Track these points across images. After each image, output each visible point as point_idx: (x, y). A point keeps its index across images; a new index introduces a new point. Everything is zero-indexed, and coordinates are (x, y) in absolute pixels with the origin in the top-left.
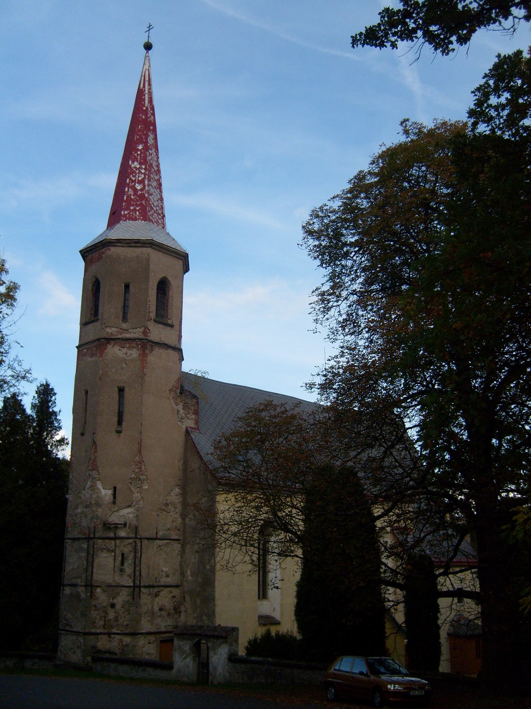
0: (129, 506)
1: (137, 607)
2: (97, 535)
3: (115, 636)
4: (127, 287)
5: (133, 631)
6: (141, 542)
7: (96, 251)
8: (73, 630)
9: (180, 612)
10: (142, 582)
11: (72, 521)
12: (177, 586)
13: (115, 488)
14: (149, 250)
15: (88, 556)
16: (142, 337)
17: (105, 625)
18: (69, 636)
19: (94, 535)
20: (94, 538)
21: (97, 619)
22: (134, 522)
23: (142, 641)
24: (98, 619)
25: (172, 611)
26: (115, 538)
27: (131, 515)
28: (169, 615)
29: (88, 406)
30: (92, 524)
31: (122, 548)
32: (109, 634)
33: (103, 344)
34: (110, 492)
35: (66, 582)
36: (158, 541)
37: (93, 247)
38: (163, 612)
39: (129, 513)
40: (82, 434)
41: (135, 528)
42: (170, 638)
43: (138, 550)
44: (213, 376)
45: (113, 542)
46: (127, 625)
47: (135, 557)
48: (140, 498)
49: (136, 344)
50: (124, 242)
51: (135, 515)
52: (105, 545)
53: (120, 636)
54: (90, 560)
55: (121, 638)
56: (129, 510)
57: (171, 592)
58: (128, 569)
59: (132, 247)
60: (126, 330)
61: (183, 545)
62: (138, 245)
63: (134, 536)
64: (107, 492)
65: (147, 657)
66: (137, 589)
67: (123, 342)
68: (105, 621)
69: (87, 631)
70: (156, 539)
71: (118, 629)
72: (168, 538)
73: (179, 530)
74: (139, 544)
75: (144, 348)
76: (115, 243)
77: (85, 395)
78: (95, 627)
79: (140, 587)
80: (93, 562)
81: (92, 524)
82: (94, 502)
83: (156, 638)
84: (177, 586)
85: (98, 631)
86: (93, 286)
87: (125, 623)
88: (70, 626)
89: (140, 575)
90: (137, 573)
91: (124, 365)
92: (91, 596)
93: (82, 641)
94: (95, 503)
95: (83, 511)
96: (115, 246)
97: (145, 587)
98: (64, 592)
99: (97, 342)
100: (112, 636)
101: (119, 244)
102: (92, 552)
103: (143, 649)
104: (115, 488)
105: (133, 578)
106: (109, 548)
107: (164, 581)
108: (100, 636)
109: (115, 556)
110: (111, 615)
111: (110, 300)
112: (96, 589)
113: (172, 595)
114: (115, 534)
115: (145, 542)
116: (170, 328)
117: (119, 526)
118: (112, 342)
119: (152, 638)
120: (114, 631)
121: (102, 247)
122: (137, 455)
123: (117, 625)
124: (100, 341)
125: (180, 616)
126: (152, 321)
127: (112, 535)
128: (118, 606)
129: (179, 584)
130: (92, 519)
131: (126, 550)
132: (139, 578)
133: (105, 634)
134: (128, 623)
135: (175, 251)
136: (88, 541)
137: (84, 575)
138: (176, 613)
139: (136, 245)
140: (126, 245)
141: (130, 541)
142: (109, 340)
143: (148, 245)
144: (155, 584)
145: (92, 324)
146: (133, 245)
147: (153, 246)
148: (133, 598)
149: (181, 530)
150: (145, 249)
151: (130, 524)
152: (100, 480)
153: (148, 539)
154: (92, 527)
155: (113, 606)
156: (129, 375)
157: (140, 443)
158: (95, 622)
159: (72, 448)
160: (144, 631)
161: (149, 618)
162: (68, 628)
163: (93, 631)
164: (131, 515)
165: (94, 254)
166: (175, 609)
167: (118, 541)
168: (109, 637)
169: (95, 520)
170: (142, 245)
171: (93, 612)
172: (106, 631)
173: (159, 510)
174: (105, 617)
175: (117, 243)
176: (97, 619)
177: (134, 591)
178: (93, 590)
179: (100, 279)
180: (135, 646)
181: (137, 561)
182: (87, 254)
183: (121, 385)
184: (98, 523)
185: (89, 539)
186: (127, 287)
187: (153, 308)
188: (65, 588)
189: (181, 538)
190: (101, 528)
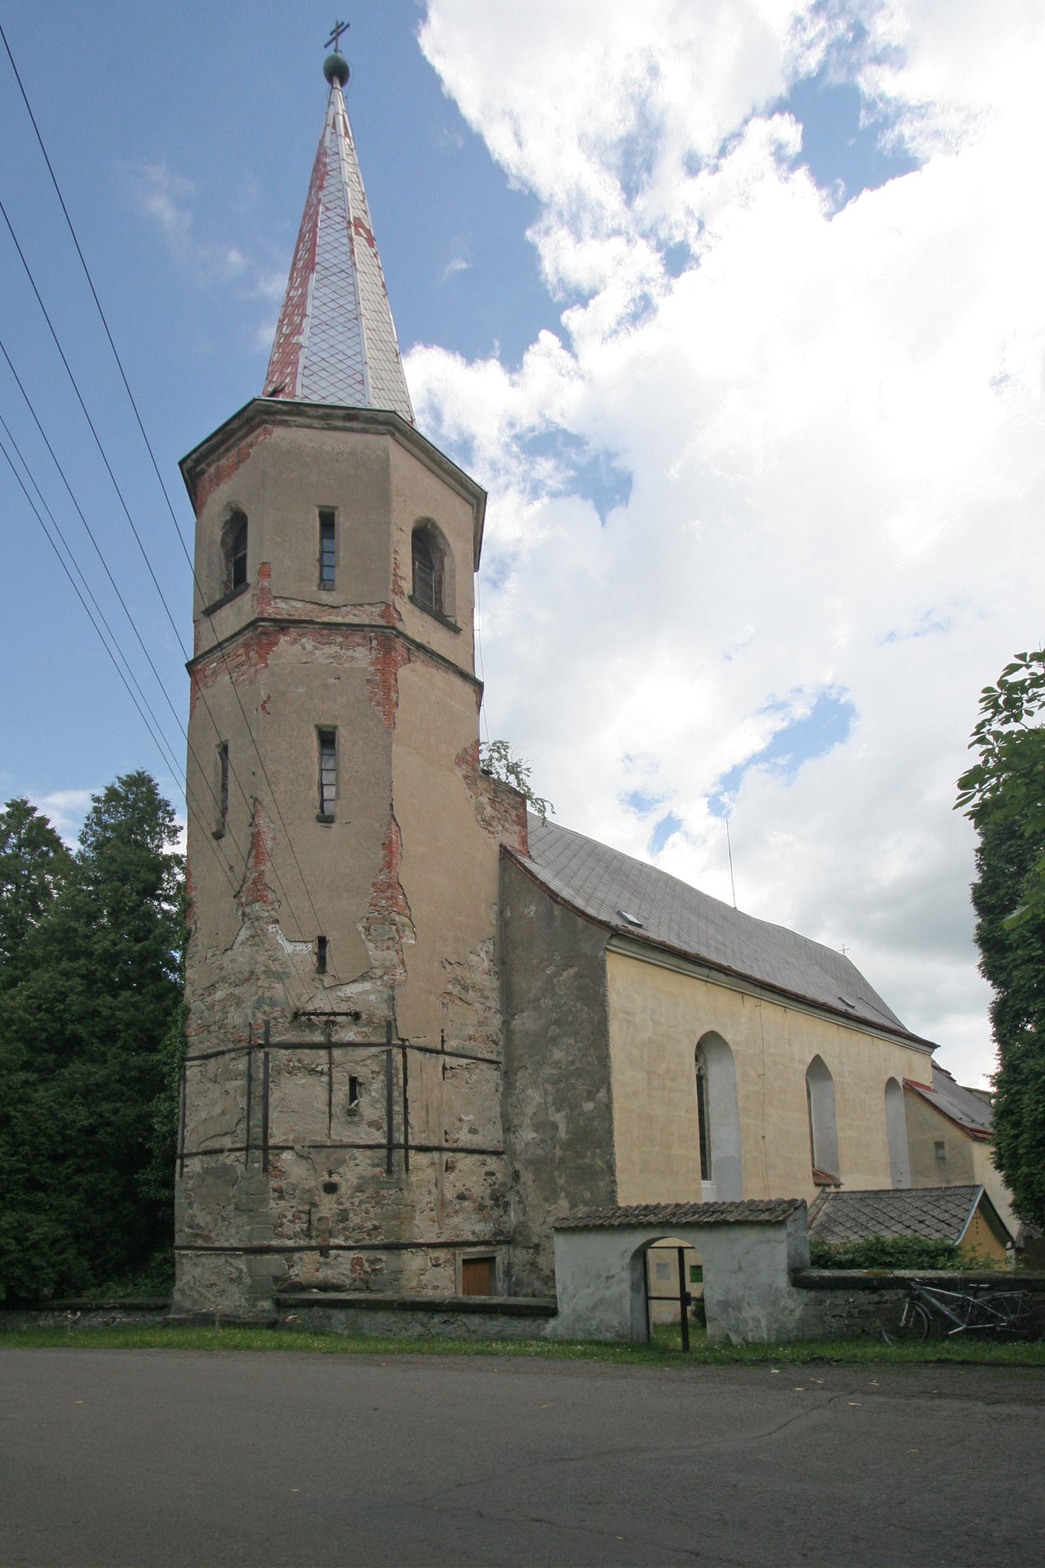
0: (364, 977)
1: (401, 1189)
2: (275, 1039)
3: (341, 1252)
4: (328, 522)
5: (392, 1240)
6: (405, 1055)
7: (228, 450)
8: (217, 1244)
9: (507, 1204)
10: (410, 1137)
11: (199, 1022)
12: (496, 1153)
13: (322, 942)
14: (387, 441)
15: (249, 1086)
16: (381, 622)
17: (309, 1229)
18: (204, 1260)
19: (267, 1039)
20: (268, 1044)
21: (285, 1217)
22: (383, 1011)
23: (414, 1262)
24: (290, 1217)
25: (489, 1202)
26: (329, 1046)
27: (373, 997)
28: (481, 1208)
29: (229, 817)
30: (259, 1015)
31: (349, 1066)
32: (324, 1250)
33: (265, 633)
34: (307, 950)
35: (190, 1147)
36: (447, 1058)
37: (219, 437)
38: (466, 1204)
39: (366, 992)
40: (218, 836)
41: (384, 1024)
42: (485, 1256)
43: (397, 1069)
44: (898, 181)
45: (323, 1053)
46: (375, 1228)
47: (389, 1085)
48: (396, 961)
49: (364, 638)
50: (312, 412)
51: (385, 996)
52: (299, 1061)
53: (355, 1252)
54: (258, 1091)
55: (359, 1255)
56: (367, 986)
57: (484, 1164)
58: (371, 1107)
59: (335, 429)
60: (332, 607)
61: (506, 1073)
62: (355, 425)
63: (384, 1040)
64: (298, 948)
65: (431, 1293)
66: (398, 1155)
67: (325, 632)
68: (309, 1222)
69: (256, 1243)
70: (442, 1052)
71: (347, 1238)
72: (468, 1054)
73: (496, 1043)
74: (398, 1058)
75: (387, 648)
76: (284, 413)
77: (222, 758)
78: (281, 1236)
79: (407, 1147)
80: (265, 1098)
81: (259, 1015)
82: (263, 969)
83: (454, 1255)
84: (496, 1153)
85: (290, 1243)
86: (225, 534)
87: (369, 1225)
88: (207, 1238)
89: (406, 1121)
90: (398, 1119)
91: (332, 681)
92: (265, 1170)
93: (243, 1267)
94: (264, 972)
95: (231, 994)
96: (284, 423)
97: (422, 1149)
98: (185, 1170)
99: (248, 634)
100: (333, 1252)
101: (299, 420)
102: (261, 1076)
103: (422, 1277)
104: (322, 942)
105: (386, 1129)
106: (314, 1066)
107: (464, 1138)
108: (296, 1256)
109: (330, 1084)
110: (328, 1206)
111: (279, 540)
112: (278, 1155)
113: (486, 1169)
114: (329, 1036)
115: (413, 1055)
116: (452, 633)
117: (340, 1019)
118: (293, 632)
119: (442, 1254)
120: (334, 1241)
121: (244, 430)
122: (382, 870)
123: (345, 1229)
124: (256, 629)
125: (506, 1212)
126: (406, 600)
127: (318, 1038)
128: (344, 1189)
129: (501, 1149)
130: (258, 1006)
131: (362, 1072)
132: (403, 1129)
133: (311, 1248)
134: (377, 1223)
135: (456, 473)
136: (249, 1054)
137: (243, 1125)
138: (498, 1206)
139: (348, 424)
140: (316, 423)
141: (374, 1050)
142: (283, 625)
143: (382, 428)
144: (445, 1145)
145: (228, 606)
146: (339, 423)
147: (397, 434)
148: (389, 1171)
149: (501, 1043)
150: (376, 437)
151: (371, 1016)
152: (277, 922)
153: (420, 1049)
154: (260, 1021)
155: (331, 1188)
156: (348, 701)
157: (388, 846)
158: (281, 1225)
159: (189, 837)
160: (421, 1241)
161: (434, 1214)
162: (200, 1243)
163: (273, 1243)
164: (373, 997)
165: (223, 461)
166: (496, 1198)
167: (337, 1053)
168: (322, 1255)
169: (267, 1008)
170: (364, 425)
171: (272, 1204)
172: (314, 1243)
173: (446, 995)
174: (309, 1213)
175: (289, 413)
176: (285, 1217)
177: (389, 1157)
178: (271, 1157)
179: (245, 509)
180: (401, 1272)
181: (396, 1094)
182: (203, 466)
183: (326, 721)
184: (276, 1014)
185: (251, 1049)
186: (328, 522)
187: (406, 569)
188: (187, 1162)
189: (501, 1059)
190: (287, 1025)
